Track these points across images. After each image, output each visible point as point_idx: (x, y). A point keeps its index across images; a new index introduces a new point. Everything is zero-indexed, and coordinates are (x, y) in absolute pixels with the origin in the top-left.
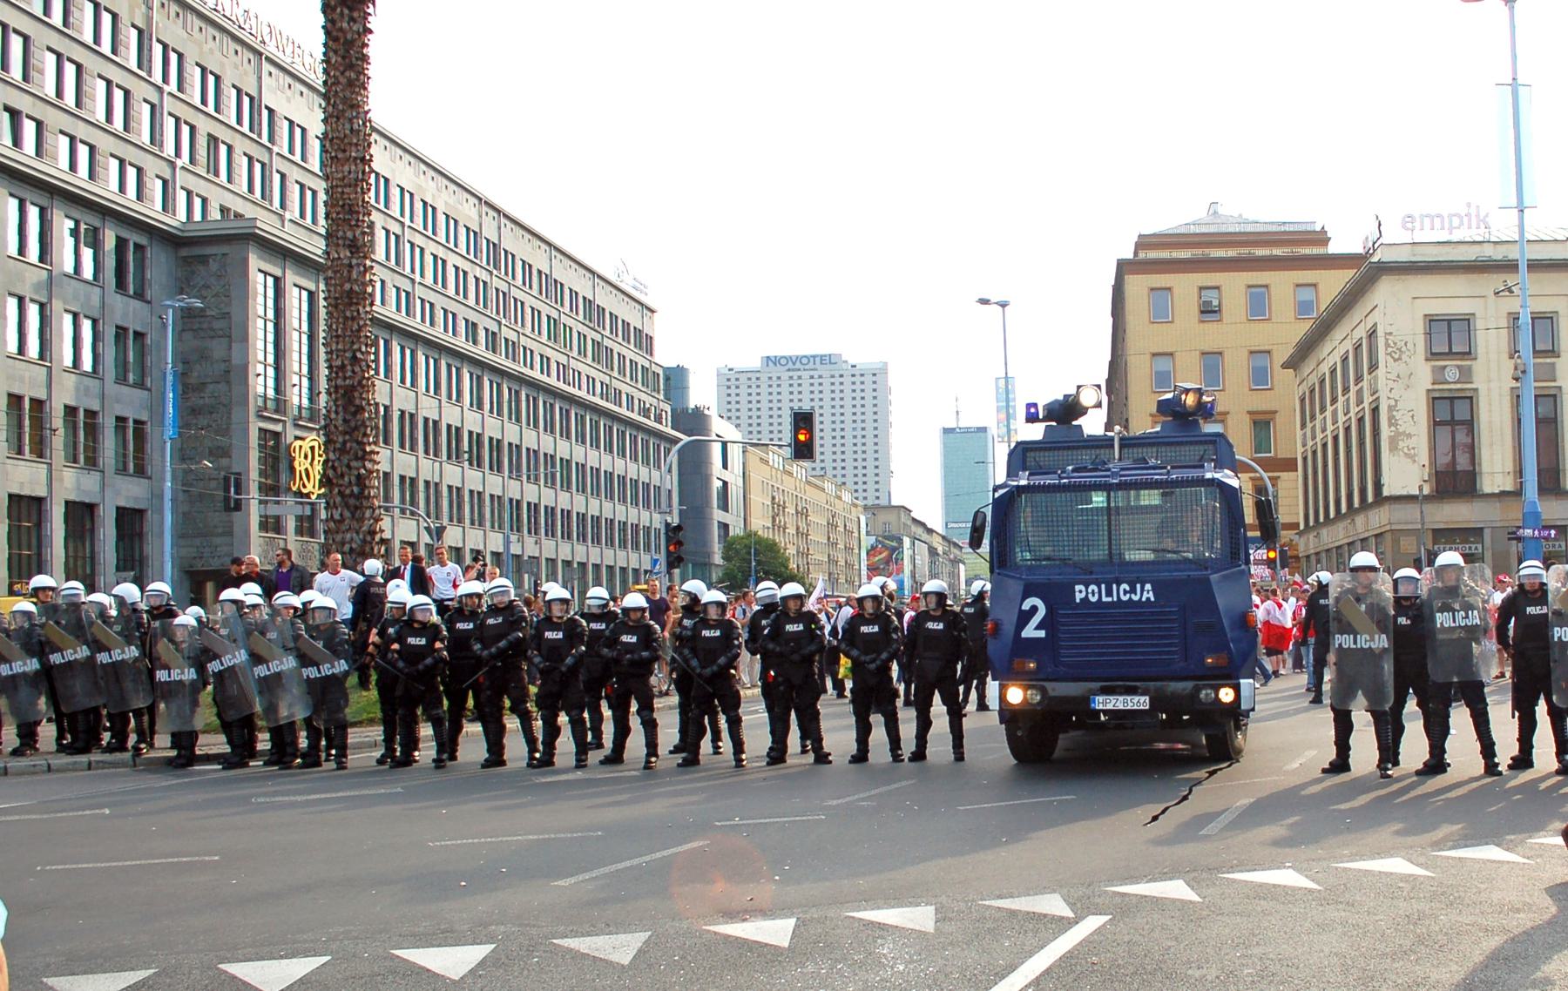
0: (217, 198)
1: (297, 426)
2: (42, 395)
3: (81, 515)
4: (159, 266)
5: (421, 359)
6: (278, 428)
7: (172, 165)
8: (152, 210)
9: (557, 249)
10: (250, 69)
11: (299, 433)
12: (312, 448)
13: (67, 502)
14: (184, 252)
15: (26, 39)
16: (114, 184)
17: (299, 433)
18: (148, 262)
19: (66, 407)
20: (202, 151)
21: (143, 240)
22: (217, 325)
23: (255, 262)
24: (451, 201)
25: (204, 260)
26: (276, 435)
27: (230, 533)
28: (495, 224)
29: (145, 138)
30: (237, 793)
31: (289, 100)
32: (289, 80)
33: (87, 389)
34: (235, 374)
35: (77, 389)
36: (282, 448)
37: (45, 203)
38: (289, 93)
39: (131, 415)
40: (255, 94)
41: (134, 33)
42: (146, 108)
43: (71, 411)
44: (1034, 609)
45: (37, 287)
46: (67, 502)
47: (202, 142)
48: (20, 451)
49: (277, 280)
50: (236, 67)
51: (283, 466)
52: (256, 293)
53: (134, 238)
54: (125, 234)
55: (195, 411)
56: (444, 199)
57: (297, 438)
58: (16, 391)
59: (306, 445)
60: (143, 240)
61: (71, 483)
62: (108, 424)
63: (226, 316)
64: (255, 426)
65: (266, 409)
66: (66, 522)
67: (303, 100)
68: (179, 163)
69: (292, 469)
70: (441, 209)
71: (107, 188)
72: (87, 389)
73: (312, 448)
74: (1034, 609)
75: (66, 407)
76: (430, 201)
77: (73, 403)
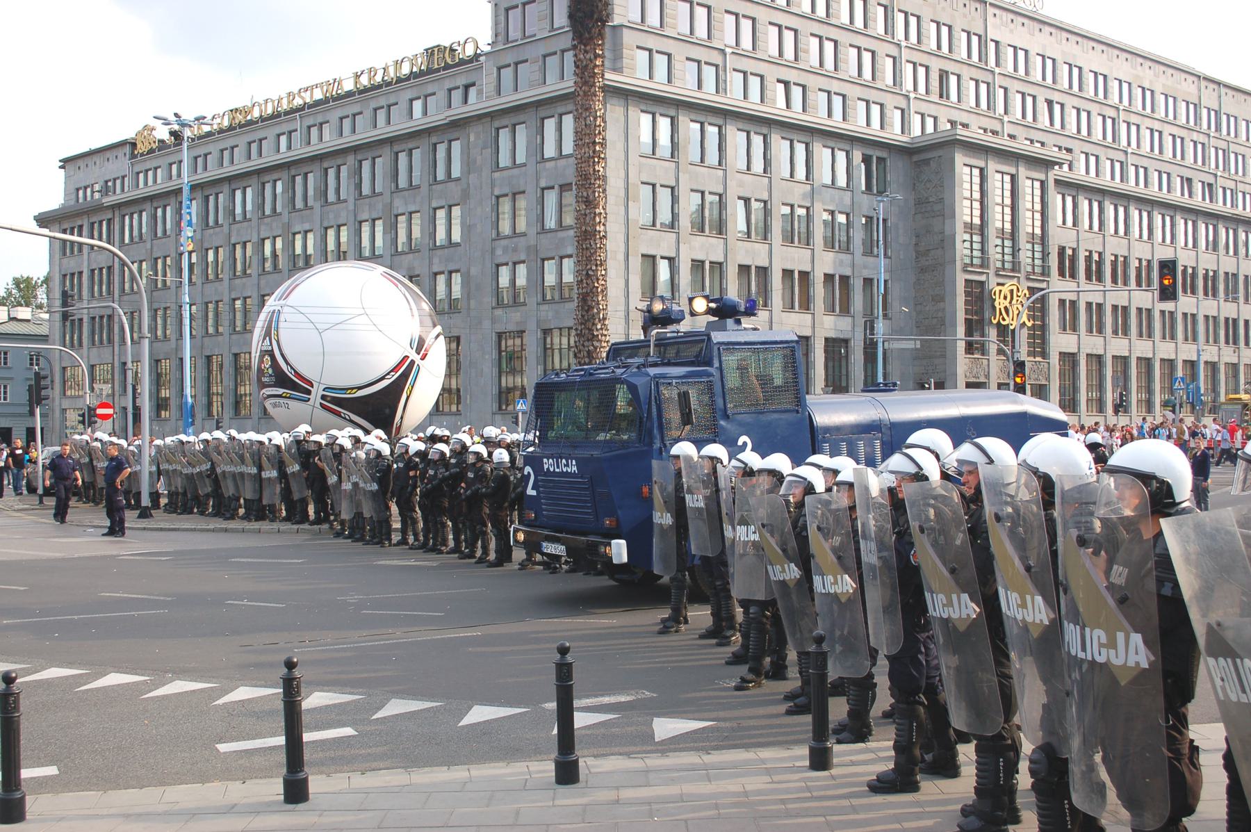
0: (944, 115)
1: (998, 275)
2: (807, 268)
3: (836, 346)
4: (896, 170)
5: (1222, 232)
6: (983, 278)
7: (1126, 152)
8: (894, 133)
9: (1226, 86)
10: (978, 15)
11: (1001, 280)
12: (1012, 291)
13: (826, 339)
14: (915, 158)
15: (836, 42)
16: (781, 103)
17: (1001, 280)
18: (888, 169)
19: (825, 275)
20: (935, 83)
21: (883, 154)
22: (937, 207)
23: (960, 159)
24: (1169, 83)
25: (926, 162)
26: (982, 283)
27: (944, 356)
28: (1216, 94)
29: (890, 81)
30: (388, 562)
31: (1011, 31)
32: (1011, 16)
33: (841, 262)
34: (947, 242)
35: (835, 262)
36: (986, 292)
37: (848, 148)
38: (1012, 26)
39: (797, 267)
40: (981, 32)
41: (881, 10)
42: (889, 61)
43: (829, 278)
44: (745, 444)
45: (804, 196)
46: (826, 339)
47: (935, 77)
48: (1065, 330)
49: (982, 170)
50: (965, 16)
51: (987, 306)
52: (962, 182)
53: (876, 153)
54: (869, 152)
55: (923, 270)
56: (1159, 81)
57: (999, 284)
58: (789, 267)
59: (1005, 290)
60: (883, 154)
61: (828, 325)
62: (857, 285)
63: (941, 200)
64: (961, 279)
65: (1004, 269)
66: (826, 351)
67: (1025, 29)
68: (1130, 151)
69: (994, 308)
70: (1158, 89)
71: (857, 124)
72: (841, 262)
73: (1012, 291)
74: (745, 444)
75: (825, 275)
76: (1146, 85)
77: (831, 272)
